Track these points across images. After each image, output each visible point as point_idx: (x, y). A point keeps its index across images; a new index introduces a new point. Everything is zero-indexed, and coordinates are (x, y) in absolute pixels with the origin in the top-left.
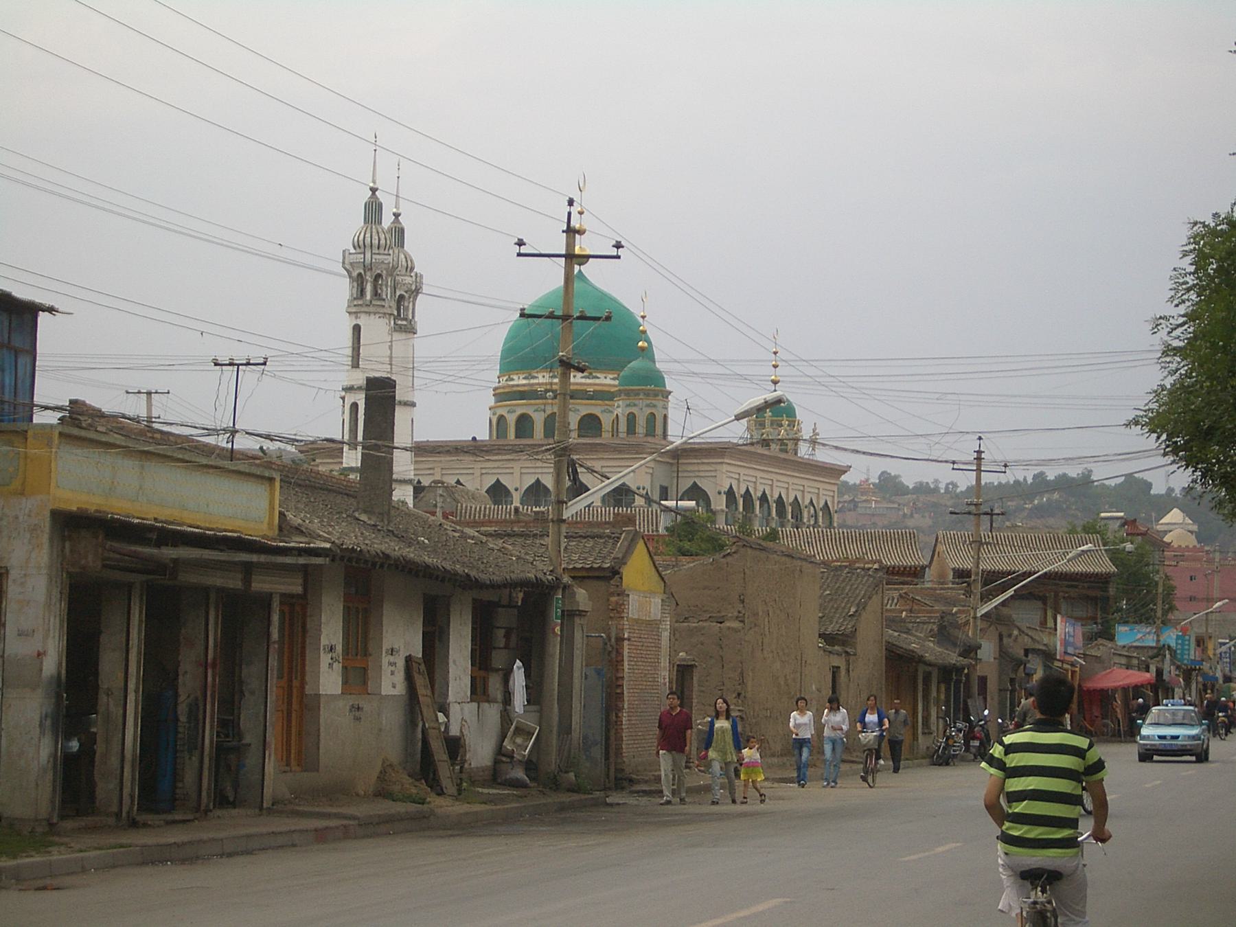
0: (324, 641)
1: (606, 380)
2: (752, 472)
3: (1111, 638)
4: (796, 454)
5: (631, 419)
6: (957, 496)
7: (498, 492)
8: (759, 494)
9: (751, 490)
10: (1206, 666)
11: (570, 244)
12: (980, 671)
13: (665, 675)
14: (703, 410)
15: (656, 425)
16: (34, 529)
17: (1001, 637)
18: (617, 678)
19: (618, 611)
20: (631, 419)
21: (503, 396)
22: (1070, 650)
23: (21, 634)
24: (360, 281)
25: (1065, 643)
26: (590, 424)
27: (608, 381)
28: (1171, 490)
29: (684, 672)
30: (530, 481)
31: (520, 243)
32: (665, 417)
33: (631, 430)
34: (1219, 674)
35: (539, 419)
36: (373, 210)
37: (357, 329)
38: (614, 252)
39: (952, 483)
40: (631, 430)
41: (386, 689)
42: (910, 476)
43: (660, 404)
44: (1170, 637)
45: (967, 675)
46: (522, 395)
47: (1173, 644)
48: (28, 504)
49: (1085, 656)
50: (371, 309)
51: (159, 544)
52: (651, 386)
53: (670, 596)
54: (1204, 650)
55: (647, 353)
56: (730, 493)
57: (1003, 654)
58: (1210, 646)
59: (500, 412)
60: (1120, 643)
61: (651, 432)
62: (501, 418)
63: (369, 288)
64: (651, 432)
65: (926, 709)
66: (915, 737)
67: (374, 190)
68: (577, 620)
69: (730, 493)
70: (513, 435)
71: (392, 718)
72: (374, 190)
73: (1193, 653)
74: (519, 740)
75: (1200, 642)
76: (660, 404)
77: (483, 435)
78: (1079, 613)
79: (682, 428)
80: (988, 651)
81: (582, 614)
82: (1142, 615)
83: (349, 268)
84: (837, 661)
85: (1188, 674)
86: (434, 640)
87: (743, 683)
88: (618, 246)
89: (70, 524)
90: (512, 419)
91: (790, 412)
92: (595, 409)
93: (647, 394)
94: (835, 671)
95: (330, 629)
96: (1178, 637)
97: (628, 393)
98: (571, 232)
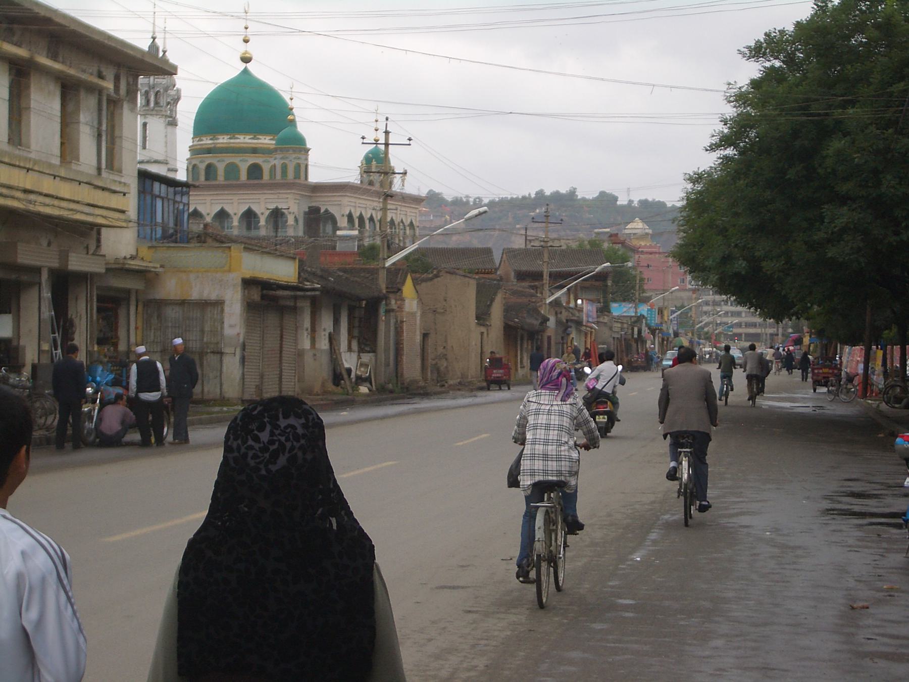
0: (305, 326)
1: (266, 141)
2: (363, 202)
4: (390, 187)
5: (284, 168)
7: (222, 215)
8: (369, 216)
9: (374, 216)
10: (664, 327)
11: (387, 138)
13: (418, 338)
14: (332, 159)
15: (302, 169)
17: (556, 313)
19: (401, 308)
20: (284, 168)
22: (590, 320)
23: (231, 326)
25: (588, 316)
26: (255, 171)
27: (267, 141)
28: (631, 202)
29: (425, 336)
31: (363, 138)
32: (307, 166)
34: (671, 331)
35: (221, 168)
38: (408, 142)
39: (478, 198)
43: (303, 157)
44: (643, 310)
46: (209, 151)
47: (646, 315)
49: (598, 323)
50: (154, 112)
52: (298, 145)
53: (420, 300)
54: (662, 317)
55: (293, 122)
56: (350, 217)
57: (559, 322)
58: (665, 313)
59: (194, 162)
61: (297, 175)
62: (195, 166)
63: (152, 99)
64: (297, 175)
65: (521, 354)
66: (516, 370)
67: (154, 38)
68: (392, 314)
69: (350, 217)
71: (325, 359)
72: (154, 38)
73: (655, 320)
74: (362, 369)
75: (661, 312)
76: (303, 157)
78: (590, 297)
80: (552, 323)
81: (393, 310)
82: (626, 298)
84: (483, 329)
85: (653, 331)
86: (336, 322)
87: (446, 341)
88: (410, 139)
89: (249, 283)
90: (202, 167)
92: (258, 160)
93: (294, 151)
94: (482, 333)
96: (648, 310)
97: (281, 150)
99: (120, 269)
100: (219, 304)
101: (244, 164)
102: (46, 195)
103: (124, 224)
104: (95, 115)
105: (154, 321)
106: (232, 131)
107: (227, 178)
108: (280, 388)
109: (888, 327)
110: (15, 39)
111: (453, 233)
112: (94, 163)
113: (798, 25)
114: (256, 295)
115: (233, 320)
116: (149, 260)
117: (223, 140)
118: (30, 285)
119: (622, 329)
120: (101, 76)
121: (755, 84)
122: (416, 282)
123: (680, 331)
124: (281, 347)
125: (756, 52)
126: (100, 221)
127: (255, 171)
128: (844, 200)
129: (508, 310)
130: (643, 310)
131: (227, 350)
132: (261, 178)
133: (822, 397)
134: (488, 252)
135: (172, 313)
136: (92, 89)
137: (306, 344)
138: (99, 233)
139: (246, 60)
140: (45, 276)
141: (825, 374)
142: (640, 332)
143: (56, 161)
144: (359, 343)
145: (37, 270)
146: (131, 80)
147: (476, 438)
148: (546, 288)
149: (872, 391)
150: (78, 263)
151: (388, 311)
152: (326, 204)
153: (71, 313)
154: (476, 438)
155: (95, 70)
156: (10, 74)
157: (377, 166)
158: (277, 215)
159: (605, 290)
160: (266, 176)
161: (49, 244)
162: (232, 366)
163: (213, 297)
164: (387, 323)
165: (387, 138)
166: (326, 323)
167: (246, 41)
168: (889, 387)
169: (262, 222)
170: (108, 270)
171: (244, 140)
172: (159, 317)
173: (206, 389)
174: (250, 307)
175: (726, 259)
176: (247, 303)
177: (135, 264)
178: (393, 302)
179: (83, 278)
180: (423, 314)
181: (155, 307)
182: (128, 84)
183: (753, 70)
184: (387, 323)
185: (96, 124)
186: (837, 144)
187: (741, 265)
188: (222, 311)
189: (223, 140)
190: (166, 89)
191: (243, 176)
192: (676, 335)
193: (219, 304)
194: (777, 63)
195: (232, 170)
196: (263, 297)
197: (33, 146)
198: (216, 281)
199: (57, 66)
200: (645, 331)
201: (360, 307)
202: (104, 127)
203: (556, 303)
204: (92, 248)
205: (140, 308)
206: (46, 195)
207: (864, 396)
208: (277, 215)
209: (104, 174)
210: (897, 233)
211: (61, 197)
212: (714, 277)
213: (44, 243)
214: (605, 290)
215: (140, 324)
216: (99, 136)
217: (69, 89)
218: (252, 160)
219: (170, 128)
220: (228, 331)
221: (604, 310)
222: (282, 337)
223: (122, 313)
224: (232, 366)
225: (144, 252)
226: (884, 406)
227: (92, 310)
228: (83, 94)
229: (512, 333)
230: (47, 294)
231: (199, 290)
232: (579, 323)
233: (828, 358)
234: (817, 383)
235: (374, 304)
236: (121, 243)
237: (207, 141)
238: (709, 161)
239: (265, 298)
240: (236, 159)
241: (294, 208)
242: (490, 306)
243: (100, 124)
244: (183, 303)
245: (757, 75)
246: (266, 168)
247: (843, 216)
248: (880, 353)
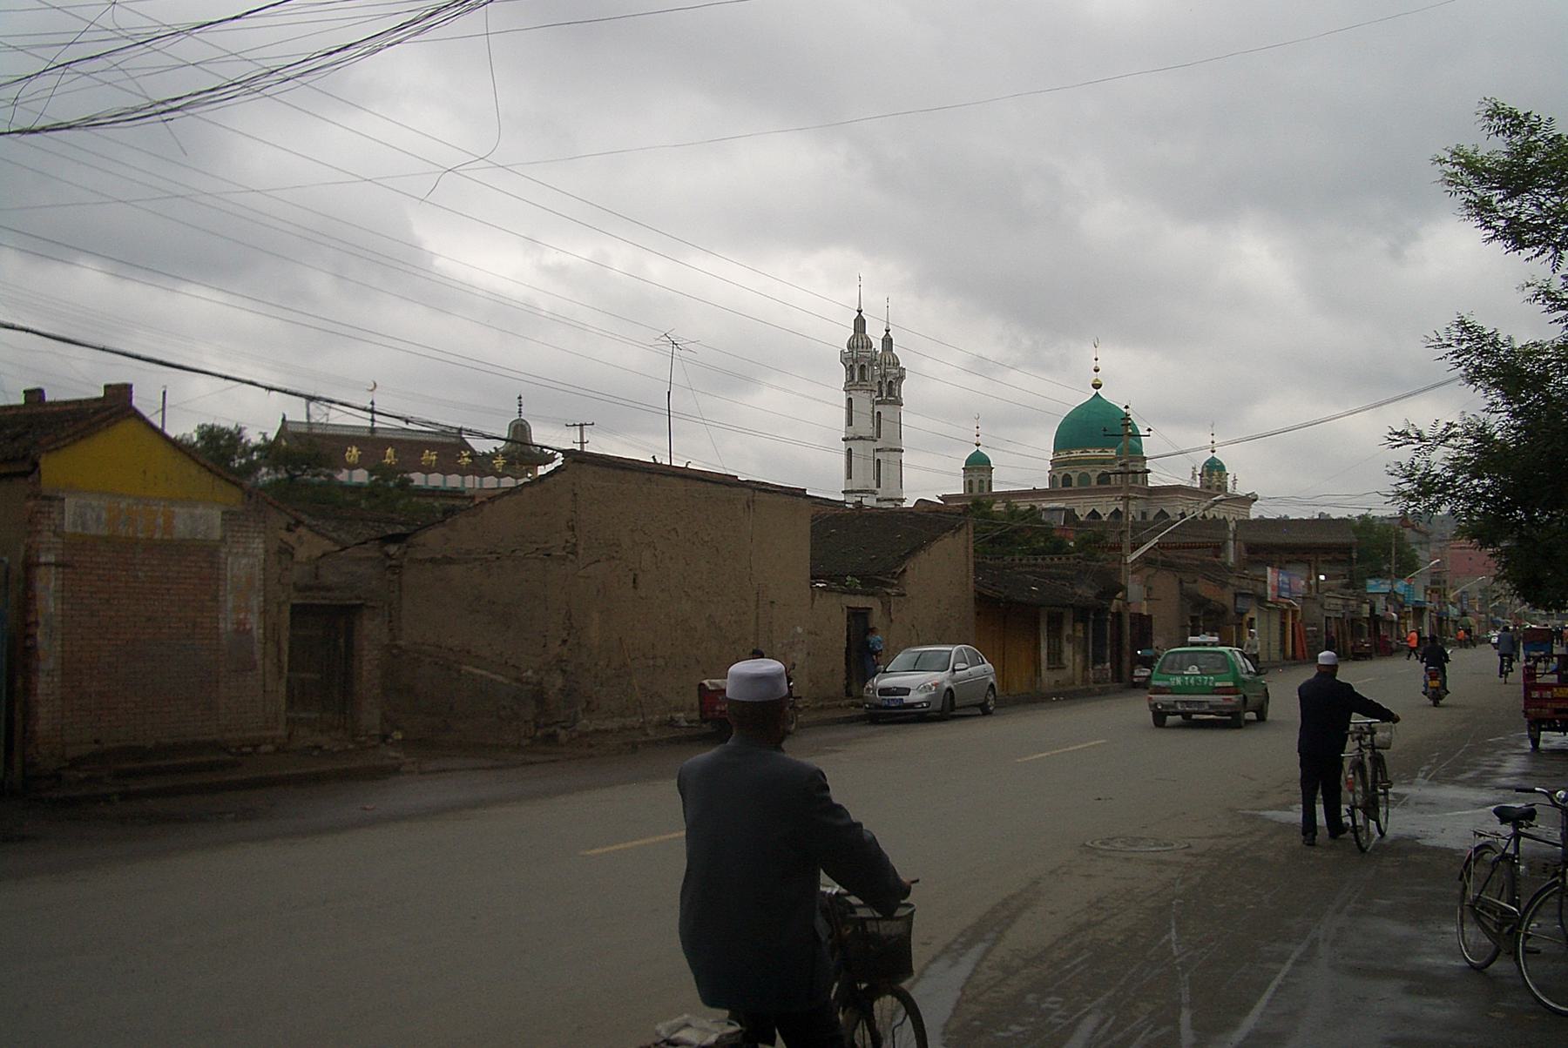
7: (1094, 514)
14: (1169, 461)
18: (28, 625)
24: (850, 370)
30: (1112, 510)
35: (1074, 477)
37: (850, 400)
42: (1336, 514)
45: (1118, 615)
79: (1158, 477)
90: (1060, 477)
101: (1094, 473)
106: (1084, 446)
107: (1080, 483)
117: (1076, 453)
139: (1097, 386)
147: (622, 846)
154: (622, 846)
171: (1094, 453)
189: (1076, 453)
191: (1094, 482)
195: (1084, 478)
237: (1063, 455)
240: (1088, 470)
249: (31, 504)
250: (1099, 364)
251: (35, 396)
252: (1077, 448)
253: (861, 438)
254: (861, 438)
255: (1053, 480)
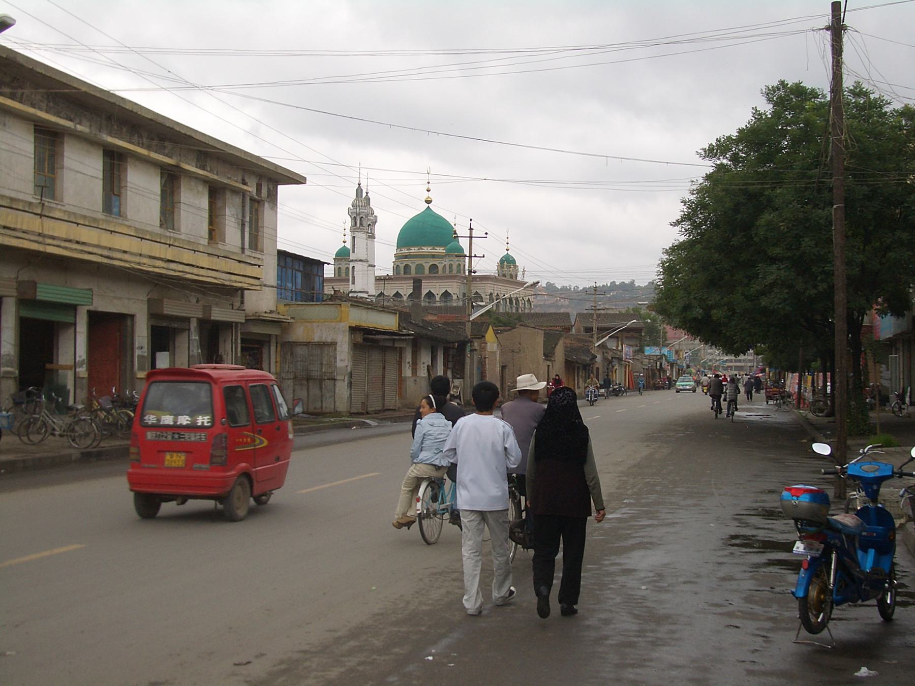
1: (440, 250)
3: (643, 352)
5: (451, 266)
6: (578, 292)
7: (397, 295)
11: (471, 233)
12: (597, 366)
13: (498, 369)
16: (344, 332)
19: (484, 349)
20: (451, 266)
21: (397, 257)
25: (626, 354)
26: (434, 268)
29: (503, 368)
33: (451, 271)
36: (359, 191)
37: (354, 237)
40: (451, 271)
41: (423, 375)
44: (665, 351)
46: (406, 257)
48: (342, 324)
51: (375, 335)
53: (499, 344)
57: (605, 359)
60: (646, 354)
61: (459, 271)
64: (459, 271)
70: (402, 270)
73: (673, 357)
75: (677, 352)
77: (391, 273)
80: (599, 358)
82: (656, 344)
83: (350, 213)
84: (549, 363)
85: (672, 365)
86: (434, 359)
89: (354, 330)
91: (514, 262)
95: (408, 357)
98: (471, 229)
99: (258, 320)
100: (333, 344)
102: (187, 265)
103: (258, 288)
104: (240, 210)
105: (289, 357)
108: (384, 404)
109: (815, 361)
110: (166, 151)
111: (540, 304)
112: (239, 244)
113: (741, 131)
114: (359, 338)
115: (343, 356)
116: (284, 313)
117: (414, 250)
118: (182, 330)
119: (649, 363)
120: (244, 183)
121: (708, 177)
122: (496, 333)
123: (692, 364)
124: (384, 377)
125: (710, 152)
126: (245, 286)
127: (434, 268)
128: (773, 260)
129: (569, 351)
130: (665, 351)
131: (338, 378)
132: (437, 272)
133: (771, 407)
134: (567, 315)
135: (300, 351)
136: (236, 191)
137: (407, 372)
138: (242, 296)
139: (428, 202)
140: (194, 324)
141: (778, 394)
142: (661, 364)
143: (205, 242)
144: (453, 372)
145: (187, 320)
146: (271, 187)
148: (595, 337)
149: (804, 403)
150: (218, 314)
151: (472, 351)
152: (477, 288)
153: (221, 351)
155: (240, 178)
156: (161, 178)
157: (507, 262)
158: (446, 295)
159: (640, 339)
160: (440, 272)
161: (197, 301)
162: (342, 389)
163: (329, 340)
164: (472, 359)
165: (471, 233)
166: (425, 359)
167: (428, 191)
168: (815, 401)
169: (438, 298)
170: (246, 320)
171: (427, 250)
172: (292, 354)
173: (324, 406)
174: (356, 347)
175: (687, 308)
176: (152, 326)
177: (274, 316)
178: (476, 344)
179: (229, 325)
180: (502, 353)
181: (288, 347)
182: (269, 189)
183: (708, 167)
184: (472, 359)
185: (240, 216)
186: (767, 216)
187: (698, 312)
188: (335, 349)
189: (414, 250)
190: (367, 216)
192: (688, 367)
193: (333, 344)
194: (725, 161)
196: (365, 340)
197: (183, 230)
198: (329, 328)
199: (201, 172)
200: (665, 365)
201: (454, 348)
202: (247, 219)
203: (603, 346)
204: (237, 304)
205: (279, 345)
206: (187, 265)
207: (799, 408)
208: (446, 295)
209: (247, 252)
210: (815, 287)
211: (205, 267)
212: (677, 321)
213: (194, 301)
214: (640, 339)
215: (278, 360)
216: (243, 225)
217: (216, 192)
218: (432, 262)
219: (369, 241)
220: (340, 364)
221: (641, 351)
222: (384, 368)
223: (265, 351)
224: (342, 389)
225: (282, 308)
226: (811, 416)
227: (236, 348)
228: (228, 195)
229: (570, 365)
230: (195, 337)
231: (318, 335)
232: (620, 359)
233: (778, 383)
234: (769, 398)
235: (463, 345)
236: (263, 301)
237: (405, 251)
238: (677, 236)
239: (367, 340)
241: (457, 291)
242: (554, 348)
243: (243, 216)
244: (307, 344)
245: (711, 170)
246: (440, 267)
247: (774, 273)
248: (810, 378)
249: (818, 317)
250: (430, 186)
251: (633, 282)
252: (429, 246)
253: (361, 260)
254: (361, 260)
255: (396, 268)
